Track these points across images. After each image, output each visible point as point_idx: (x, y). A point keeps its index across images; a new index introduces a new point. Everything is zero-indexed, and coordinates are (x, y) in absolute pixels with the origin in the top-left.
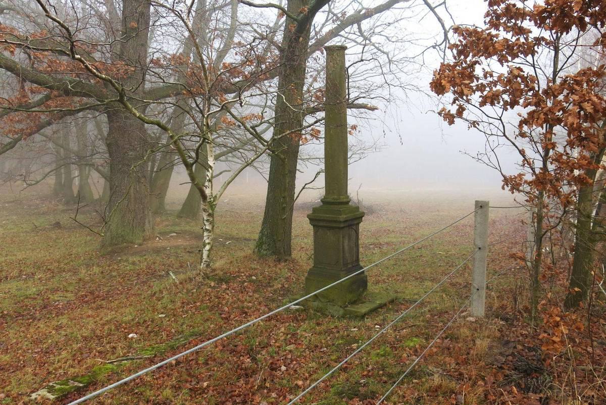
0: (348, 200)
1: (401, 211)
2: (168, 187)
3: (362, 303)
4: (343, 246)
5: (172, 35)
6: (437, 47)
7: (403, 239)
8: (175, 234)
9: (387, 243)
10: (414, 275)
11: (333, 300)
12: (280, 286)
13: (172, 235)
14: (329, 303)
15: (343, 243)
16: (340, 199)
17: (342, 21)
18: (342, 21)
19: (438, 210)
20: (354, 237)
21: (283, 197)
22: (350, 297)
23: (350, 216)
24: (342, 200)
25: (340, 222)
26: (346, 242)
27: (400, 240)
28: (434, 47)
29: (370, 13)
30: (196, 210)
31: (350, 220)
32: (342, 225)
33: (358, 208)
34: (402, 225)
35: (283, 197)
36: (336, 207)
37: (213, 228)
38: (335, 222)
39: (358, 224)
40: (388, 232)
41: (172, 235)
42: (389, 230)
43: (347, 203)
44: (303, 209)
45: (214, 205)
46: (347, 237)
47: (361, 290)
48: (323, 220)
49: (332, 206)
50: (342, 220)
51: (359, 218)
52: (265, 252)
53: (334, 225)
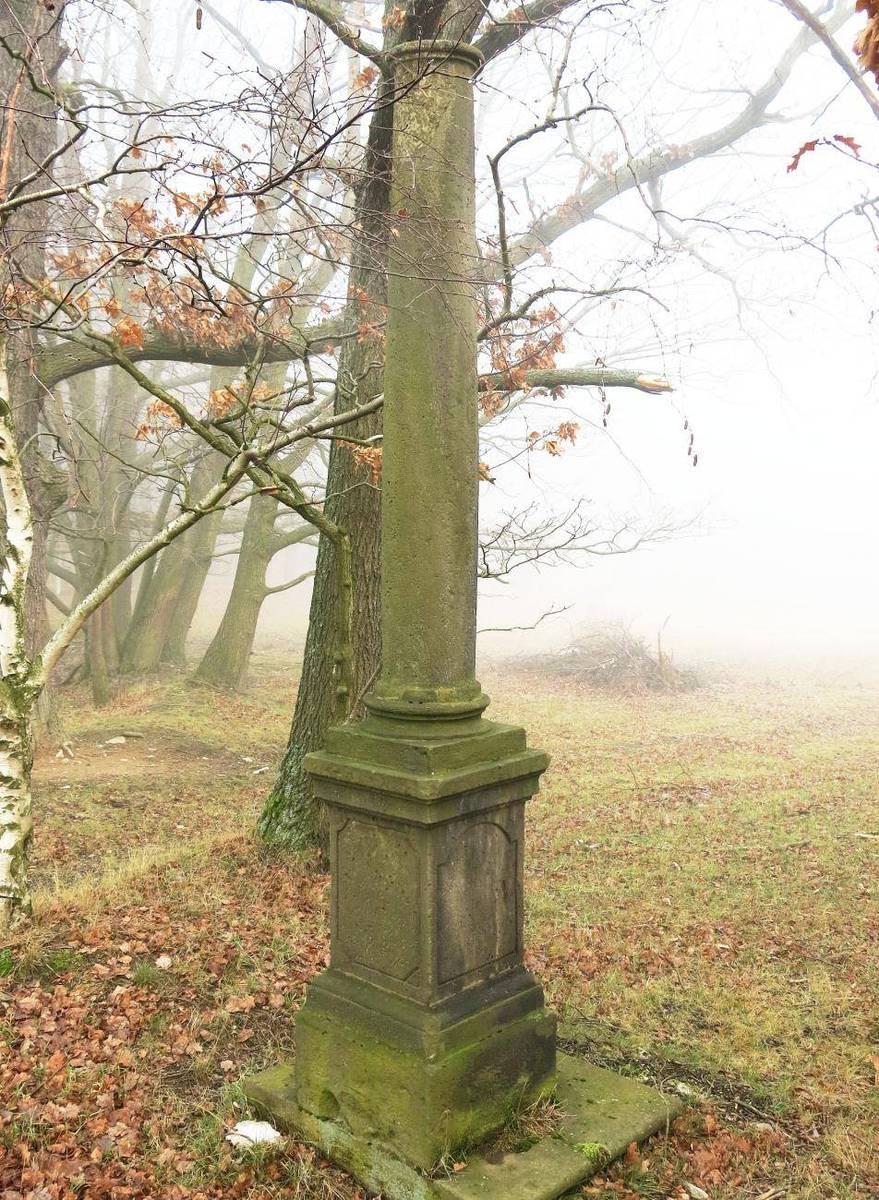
0: (475, 703)
1: (768, 684)
3: (519, 1149)
4: (440, 905)
7: (763, 771)
8: (122, 740)
11: (392, 1133)
13: (114, 741)
14: (376, 1142)
15: (439, 886)
17: (602, 177)
18: (602, 177)
19: (860, 685)
20: (500, 860)
21: (339, 663)
22: (466, 1122)
23: (472, 772)
25: (420, 803)
31: (470, 793)
32: (429, 818)
34: (767, 725)
35: (339, 663)
36: (413, 737)
37: (27, 769)
38: (408, 799)
39: (520, 803)
40: (725, 744)
41: (114, 741)
42: (727, 740)
43: (474, 714)
44: (529, 669)
46: (459, 866)
47: (524, 1079)
48: (360, 788)
49: (401, 729)
50: (426, 793)
51: (528, 778)
52: (285, 836)
53: (402, 812)
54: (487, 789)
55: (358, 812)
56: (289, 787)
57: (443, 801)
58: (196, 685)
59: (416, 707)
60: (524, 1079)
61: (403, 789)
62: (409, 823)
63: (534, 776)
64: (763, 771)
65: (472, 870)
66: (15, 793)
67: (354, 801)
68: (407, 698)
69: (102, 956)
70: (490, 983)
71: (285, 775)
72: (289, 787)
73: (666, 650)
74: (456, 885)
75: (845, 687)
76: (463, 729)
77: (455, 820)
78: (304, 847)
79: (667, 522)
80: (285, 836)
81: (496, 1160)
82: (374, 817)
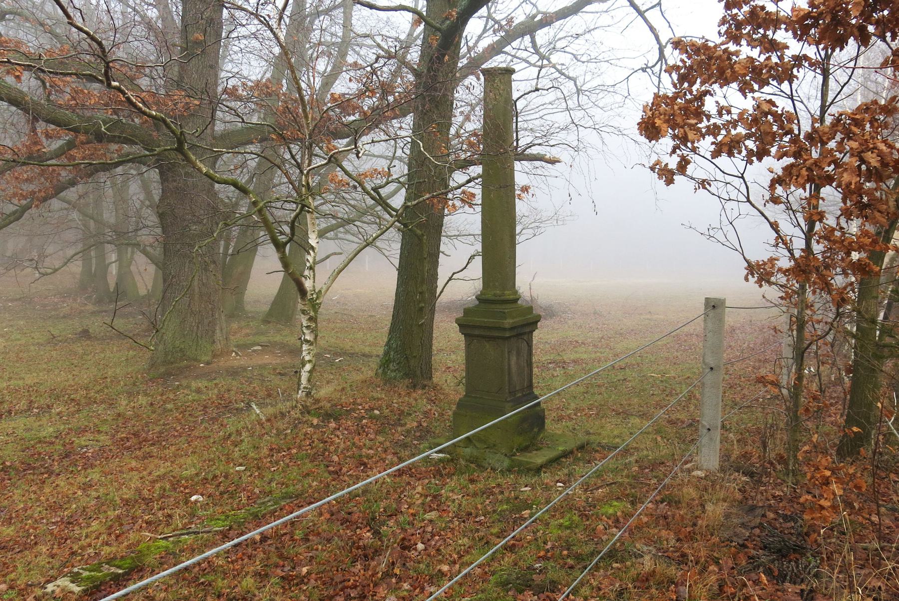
1: (594, 314)
3: (536, 450)
4: (509, 365)
7: (598, 354)
8: (260, 348)
11: (494, 445)
12: (415, 424)
13: (255, 348)
16: (504, 295)
21: (420, 293)
22: (519, 440)
23: (518, 320)
25: (505, 329)
26: (514, 359)
28: (644, 70)
33: (530, 309)
34: (597, 334)
35: (420, 293)
36: (498, 308)
37: (316, 338)
39: (531, 332)
40: (576, 344)
41: (255, 348)
42: (577, 342)
44: (449, 309)
45: (317, 304)
47: (536, 430)
48: (480, 327)
49: (493, 306)
50: (507, 326)
51: (533, 324)
52: (393, 374)
54: (523, 326)
55: (478, 336)
56: (392, 353)
57: (512, 329)
58: (269, 322)
59: (497, 298)
60: (536, 430)
61: (497, 326)
62: (498, 338)
63: (537, 322)
64: (598, 354)
65: (518, 354)
66: (311, 348)
67: (477, 332)
68: (495, 295)
69: (354, 410)
70: (524, 396)
71: (390, 348)
72: (392, 353)
73: (534, 295)
74: (514, 359)
75: (641, 314)
76: (513, 306)
77: (514, 336)
78: (402, 378)
79: (538, 218)
80: (393, 374)
81: (530, 452)
82: (483, 337)
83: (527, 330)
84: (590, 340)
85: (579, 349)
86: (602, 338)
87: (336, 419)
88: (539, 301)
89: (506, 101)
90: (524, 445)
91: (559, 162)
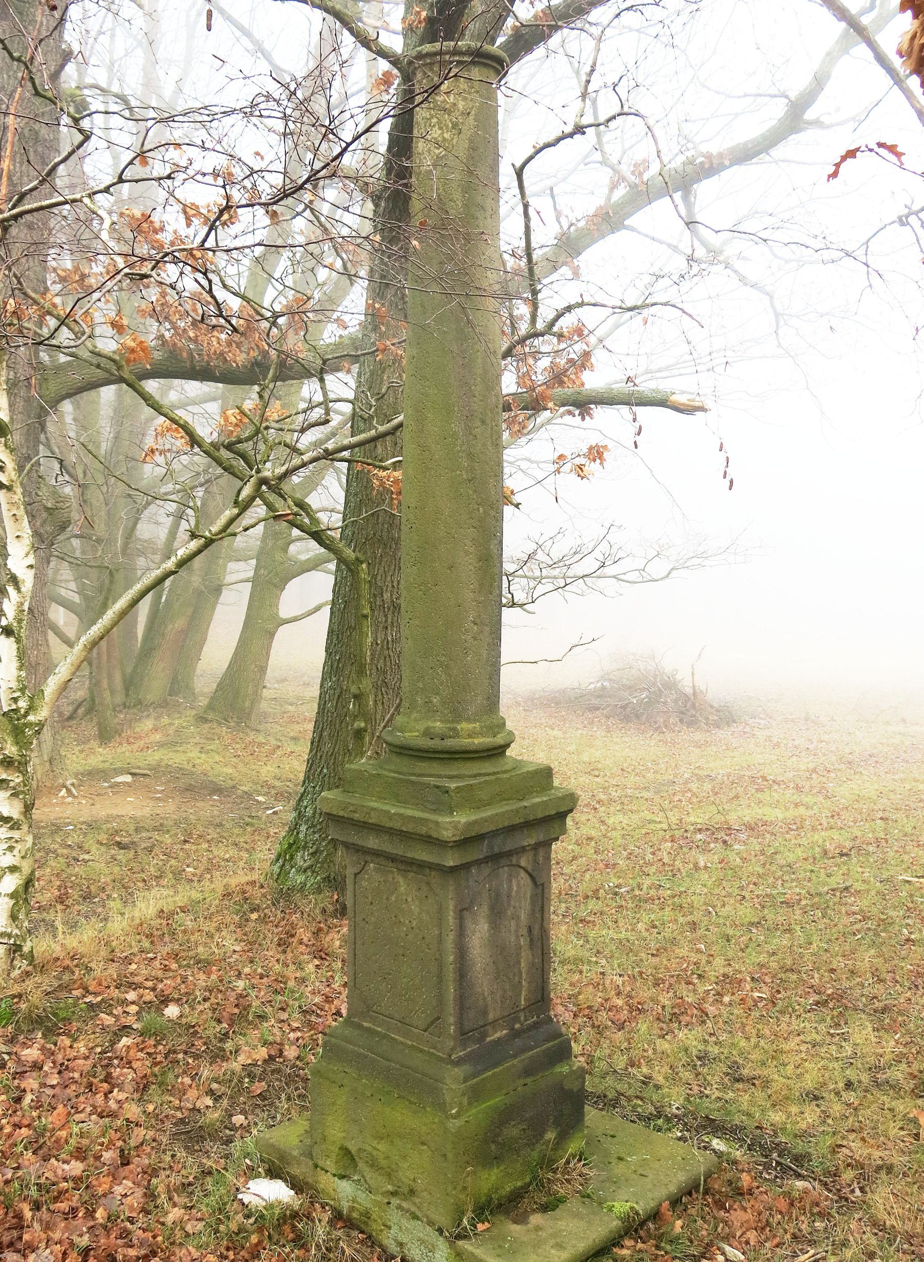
0: (500, 740)
1: (806, 719)
2: (205, 640)
4: (462, 953)
5: (25, 158)
6: (913, 220)
7: (802, 810)
8: (128, 778)
9: (750, 828)
10: (815, 981)
12: (262, 1053)
13: (120, 779)
14: (395, 1201)
15: (461, 932)
16: (456, 734)
17: (633, 186)
18: (633, 186)
20: (526, 904)
21: (356, 697)
22: (491, 1180)
24: (466, 742)
25: (441, 844)
26: (479, 931)
27: (792, 813)
28: (903, 221)
29: (715, 162)
30: (247, 704)
31: (495, 833)
33: (546, 774)
34: (807, 763)
35: (356, 697)
37: (28, 808)
38: (429, 841)
39: (547, 844)
40: (762, 783)
41: (120, 779)
42: (764, 779)
43: (498, 752)
44: (557, 703)
45: (30, 725)
46: (482, 911)
47: (550, 1135)
48: (377, 829)
49: (423, 767)
50: (447, 834)
51: (555, 818)
52: (300, 879)
53: (422, 854)
54: (511, 829)
56: (303, 828)
57: (466, 842)
58: (206, 721)
59: (436, 744)
60: (550, 1135)
61: (423, 830)
62: (432, 867)
63: (562, 816)
65: (497, 914)
66: (16, 834)
67: (372, 842)
69: (107, 1006)
70: (515, 1034)
71: (300, 815)
72: (303, 828)
74: (479, 931)
76: (487, 767)
77: (478, 862)
80: (300, 879)
81: (521, 1219)
82: (393, 859)
83: (529, 840)
84: (790, 775)
85: (765, 796)
86: (814, 771)
87: (50, 1032)
88: (709, 697)
89: (473, 148)
90: (509, 1188)
91: (702, 409)
